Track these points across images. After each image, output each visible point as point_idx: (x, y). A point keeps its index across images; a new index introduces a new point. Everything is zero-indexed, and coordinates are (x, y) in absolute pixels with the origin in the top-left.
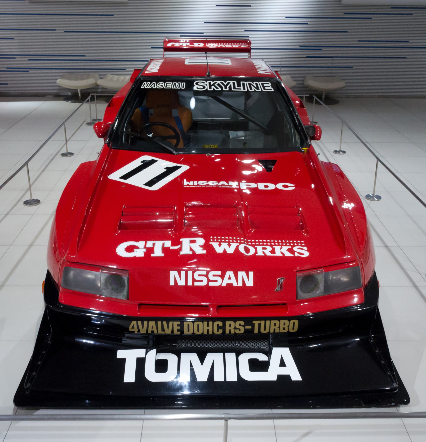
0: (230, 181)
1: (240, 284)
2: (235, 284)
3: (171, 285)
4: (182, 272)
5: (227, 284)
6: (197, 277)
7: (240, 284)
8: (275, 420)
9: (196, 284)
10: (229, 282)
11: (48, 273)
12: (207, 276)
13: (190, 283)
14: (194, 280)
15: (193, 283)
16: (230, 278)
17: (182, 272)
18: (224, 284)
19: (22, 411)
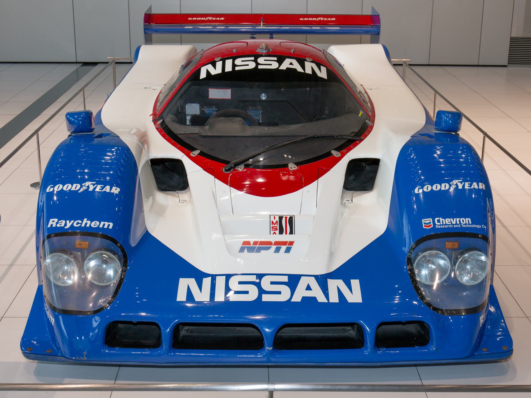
2: (321, 298)
5: (304, 298)
7: (334, 298)
10: (309, 294)
16: (309, 288)
18: (297, 298)
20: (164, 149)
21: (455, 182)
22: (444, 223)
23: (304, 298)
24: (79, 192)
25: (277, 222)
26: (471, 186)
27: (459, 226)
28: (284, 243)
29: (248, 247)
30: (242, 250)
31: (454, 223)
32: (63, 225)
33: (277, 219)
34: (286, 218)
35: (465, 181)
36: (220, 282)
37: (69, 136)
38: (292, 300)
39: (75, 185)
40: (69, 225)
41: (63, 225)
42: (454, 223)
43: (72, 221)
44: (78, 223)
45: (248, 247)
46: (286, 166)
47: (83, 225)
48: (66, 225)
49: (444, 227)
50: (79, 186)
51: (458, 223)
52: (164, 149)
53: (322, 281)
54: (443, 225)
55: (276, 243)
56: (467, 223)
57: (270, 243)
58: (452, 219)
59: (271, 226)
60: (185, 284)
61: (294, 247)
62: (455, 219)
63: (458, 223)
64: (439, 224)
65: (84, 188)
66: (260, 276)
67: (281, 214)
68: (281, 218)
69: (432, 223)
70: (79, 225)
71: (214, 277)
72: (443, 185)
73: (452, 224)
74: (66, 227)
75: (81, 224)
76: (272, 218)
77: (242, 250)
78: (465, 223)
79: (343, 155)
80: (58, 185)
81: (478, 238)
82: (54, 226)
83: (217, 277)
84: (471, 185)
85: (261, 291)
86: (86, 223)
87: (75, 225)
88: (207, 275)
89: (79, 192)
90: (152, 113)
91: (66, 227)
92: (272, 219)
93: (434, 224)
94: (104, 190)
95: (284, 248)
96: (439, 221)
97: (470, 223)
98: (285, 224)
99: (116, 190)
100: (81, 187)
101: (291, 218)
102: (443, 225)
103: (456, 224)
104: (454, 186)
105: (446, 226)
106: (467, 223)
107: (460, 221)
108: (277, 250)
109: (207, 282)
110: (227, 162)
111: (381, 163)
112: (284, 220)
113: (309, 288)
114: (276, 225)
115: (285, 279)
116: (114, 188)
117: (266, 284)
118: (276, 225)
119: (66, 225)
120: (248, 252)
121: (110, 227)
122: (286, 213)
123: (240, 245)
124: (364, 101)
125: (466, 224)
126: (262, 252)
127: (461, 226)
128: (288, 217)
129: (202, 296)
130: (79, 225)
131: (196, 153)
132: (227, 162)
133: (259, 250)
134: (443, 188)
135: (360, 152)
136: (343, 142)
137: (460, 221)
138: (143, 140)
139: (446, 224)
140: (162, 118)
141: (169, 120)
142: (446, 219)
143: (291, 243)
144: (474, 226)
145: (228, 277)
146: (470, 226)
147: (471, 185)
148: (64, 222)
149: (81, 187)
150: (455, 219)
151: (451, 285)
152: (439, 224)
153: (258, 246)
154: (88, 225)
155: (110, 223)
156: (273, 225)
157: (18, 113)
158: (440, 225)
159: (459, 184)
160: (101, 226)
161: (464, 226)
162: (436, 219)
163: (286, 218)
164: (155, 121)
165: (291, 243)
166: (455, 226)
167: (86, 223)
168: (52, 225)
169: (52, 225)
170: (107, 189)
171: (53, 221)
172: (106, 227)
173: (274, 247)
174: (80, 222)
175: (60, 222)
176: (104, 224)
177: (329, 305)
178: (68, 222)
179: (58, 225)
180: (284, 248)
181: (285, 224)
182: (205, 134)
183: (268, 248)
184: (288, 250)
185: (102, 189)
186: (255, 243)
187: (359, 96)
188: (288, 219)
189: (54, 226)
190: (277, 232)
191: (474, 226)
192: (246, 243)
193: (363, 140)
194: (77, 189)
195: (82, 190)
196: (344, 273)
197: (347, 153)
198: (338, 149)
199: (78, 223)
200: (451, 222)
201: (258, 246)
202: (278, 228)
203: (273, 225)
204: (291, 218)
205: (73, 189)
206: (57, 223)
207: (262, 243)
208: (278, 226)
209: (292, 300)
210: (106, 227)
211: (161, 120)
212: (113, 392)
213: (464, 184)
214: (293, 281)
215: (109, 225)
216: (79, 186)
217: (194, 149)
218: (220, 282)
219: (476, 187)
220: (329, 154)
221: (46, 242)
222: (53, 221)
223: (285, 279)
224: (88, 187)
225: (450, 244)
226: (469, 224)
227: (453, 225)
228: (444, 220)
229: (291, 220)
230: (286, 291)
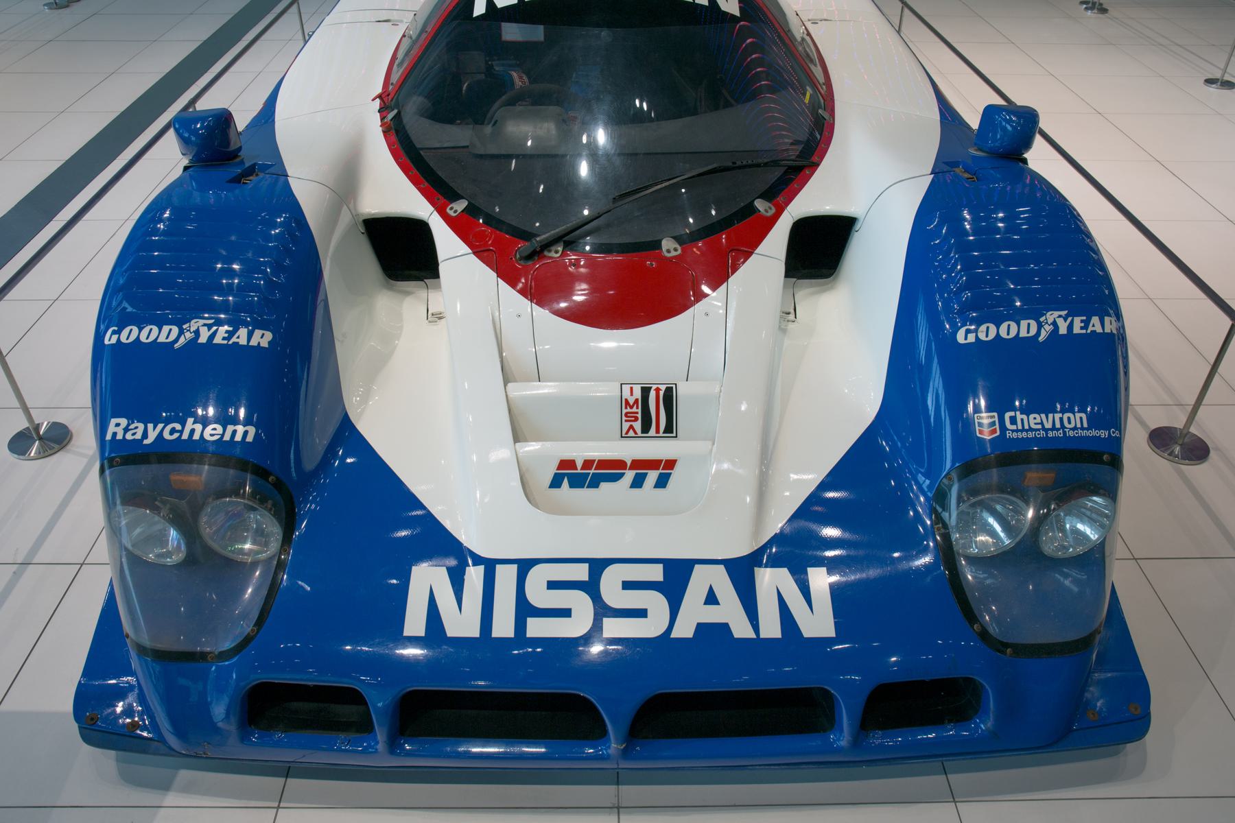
0: (500, 35)
1: (771, 628)
2: (741, 629)
3: (542, 38)
4: (421, 632)
5: (701, 627)
6: (538, 595)
7: (771, 628)
8: (90, 411)
9: (537, 628)
10: (712, 615)
11: (109, 613)
12: (591, 587)
13: (503, 627)
14: (525, 610)
15: (520, 625)
16: (711, 599)
17: (421, 632)
18: (684, 629)
19: (781, 199)
20: (393, 193)
21: (1051, 316)
22: (1026, 427)
23: (701, 627)
24: (177, 346)
25: (637, 400)
26: (1085, 327)
27: (1060, 434)
28: (653, 464)
29: (574, 475)
30: (556, 483)
31: (1048, 425)
32: (139, 436)
33: (638, 393)
34: (658, 390)
35: (1072, 314)
36: (506, 577)
37: (186, 168)
38: (674, 635)
39: (166, 328)
40: (152, 436)
41: (139, 436)
42: (1048, 425)
43: (160, 426)
44: (173, 431)
45: (574, 475)
46: (657, 245)
47: (185, 436)
48: (145, 435)
49: (1024, 435)
50: (175, 330)
51: (1058, 425)
52: (393, 193)
53: (742, 572)
54: (1023, 430)
55: (637, 464)
56: (1079, 425)
57: (620, 464)
58: (1043, 416)
59: (624, 411)
60: (427, 578)
61: (676, 474)
62: (1050, 416)
63: (1058, 425)
64: (1014, 427)
65: (189, 335)
66: (598, 566)
67: (646, 380)
68: (645, 391)
69: (997, 426)
70: (176, 435)
71: (490, 566)
72: (1024, 323)
73: (1043, 428)
74: (145, 442)
75: (181, 432)
76: (626, 389)
77: (556, 483)
78: (1072, 425)
79: (780, 211)
80: (128, 329)
81: (1102, 462)
82: (119, 437)
83: (498, 566)
84: (1086, 324)
85: (603, 611)
86: (193, 431)
87: (167, 435)
88: (478, 560)
89: (177, 346)
90: (379, 90)
91: (145, 442)
92: (626, 393)
93: (1003, 428)
94: (234, 339)
95: (652, 476)
96: (1013, 420)
97: (1085, 425)
98: (654, 410)
99: (262, 338)
100: (181, 332)
101: (669, 391)
102: (1023, 430)
103: (1054, 428)
104: (1048, 328)
105: (1031, 435)
106: (1079, 425)
107: (1061, 419)
108: (638, 483)
109: (474, 575)
110: (527, 236)
111: (857, 227)
112: (653, 394)
113: (711, 599)
114: (634, 410)
115: (656, 573)
116: (258, 333)
117: (612, 594)
118: (634, 410)
119: (145, 435)
120: (572, 486)
121: (250, 439)
122: (659, 378)
123: (551, 470)
124: (808, 55)
125: (1075, 428)
126: (603, 485)
127: (1064, 433)
128: (663, 388)
129: (462, 623)
130: (176, 435)
131: (459, 206)
132: (527, 236)
133: (594, 484)
134: (1023, 334)
135: (811, 200)
136: (777, 173)
137: (1061, 419)
138: (347, 180)
139: (1031, 429)
140: (397, 106)
141: (413, 106)
142: (1032, 416)
143: (671, 464)
144: (1093, 433)
145: (525, 566)
146: (1085, 433)
147: (1086, 324)
148: (141, 426)
149: (181, 332)
150: (1050, 416)
151: (1026, 554)
152: (1014, 427)
153: (592, 471)
154: (196, 437)
155: (248, 428)
156: (629, 410)
157: (205, 37)
158: (1017, 431)
159: (1060, 322)
160: (227, 437)
161: (1071, 434)
162: (1008, 415)
163: (658, 390)
164: (383, 110)
165: (671, 464)
166: (1050, 434)
167: (193, 431)
168: (115, 434)
169: (115, 434)
170: (242, 336)
171: (118, 425)
172: (238, 438)
173: (630, 475)
174: (178, 427)
175: (132, 426)
176: (235, 432)
177: (758, 645)
178: (150, 426)
179: (129, 436)
180: (652, 476)
181: (654, 410)
182: (482, 152)
183: (616, 478)
184: (662, 483)
185: (228, 339)
186: (588, 464)
187: (800, 48)
188: (662, 393)
189: (119, 437)
190: (638, 426)
191: (1093, 433)
192: (566, 464)
193: (818, 165)
194: (171, 338)
195: (182, 341)
196: (794, 550)
197: (787, 204)
198: (769, 195)
199: (173, 431)
200: (1042, 423)
201: (592, 471)
202: (639, 416)
203: (629, 410)
204: (669, 391)
205: (162, 339)
206: (126, 430)
207: (603, 464)
208: (639, 410)
209: (674, 635)
210: (238, 438)
211: (395, 111)
212: (293, 782)
213: (1072, 322)
214: (675, 578)
215: (246, 433)
216: (175, 330)
217: (456, 197)
218: (506, 577)
219: (1099, 329)
220: (750, 209)
221: (107, 472)
222: (118, 425)
223: (656, 573)
224: (197, 332)
225: (1034, 475)
226: (1082, 428)
227: (1046, 430)
228: (1024, 417)
229: (669, 397)
230: (656, 603)
